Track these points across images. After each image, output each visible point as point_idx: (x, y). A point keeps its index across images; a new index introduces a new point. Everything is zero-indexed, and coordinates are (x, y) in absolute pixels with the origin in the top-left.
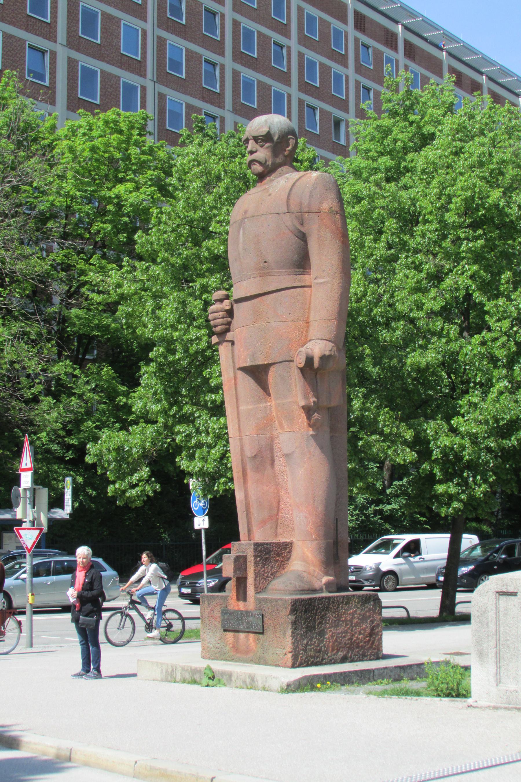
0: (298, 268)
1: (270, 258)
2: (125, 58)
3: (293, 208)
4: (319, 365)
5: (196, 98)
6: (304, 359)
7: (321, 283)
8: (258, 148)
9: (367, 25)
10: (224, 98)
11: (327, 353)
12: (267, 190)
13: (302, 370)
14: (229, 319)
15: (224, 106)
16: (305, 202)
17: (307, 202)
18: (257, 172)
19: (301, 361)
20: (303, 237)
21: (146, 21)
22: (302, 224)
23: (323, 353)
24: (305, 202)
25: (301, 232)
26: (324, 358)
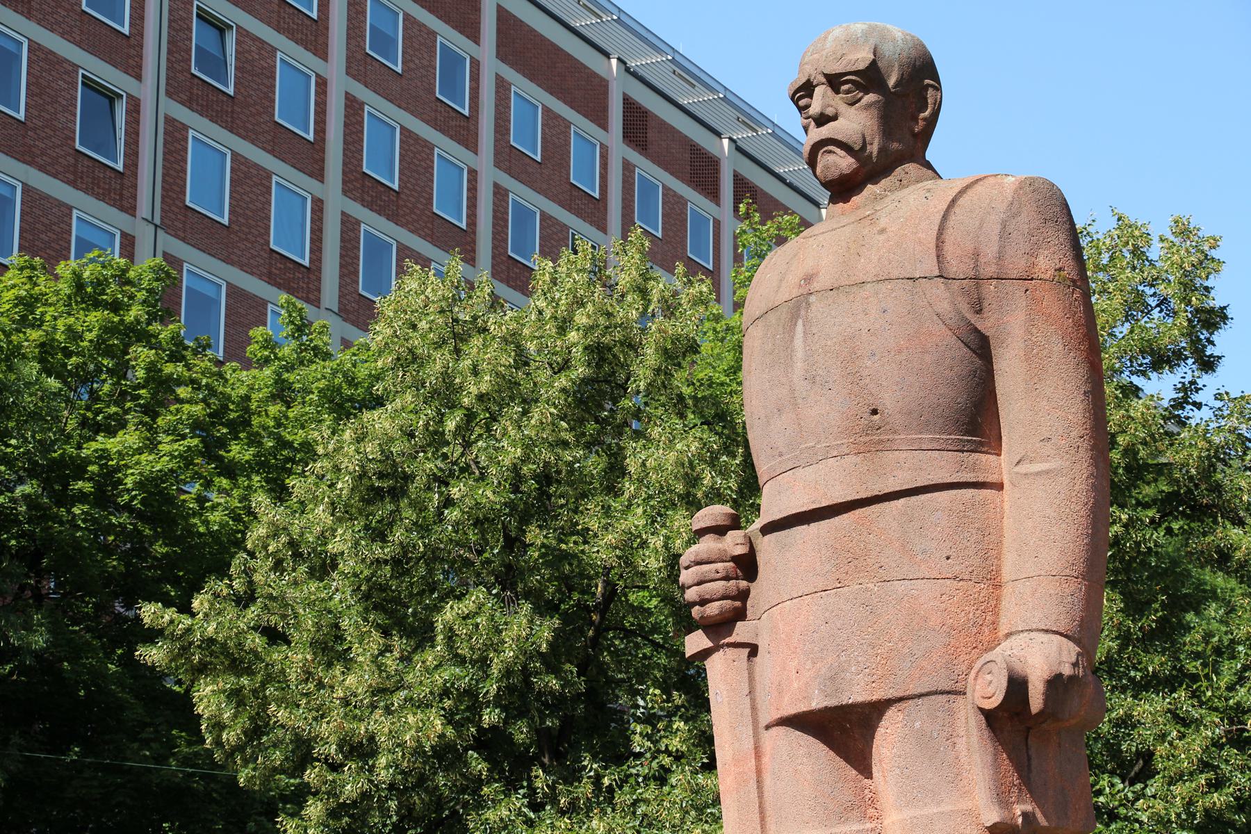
0: (967, 433)
1: (889, 401)
2: (86, 162)
3: (956, 266)
4: (1046, 701)
5: (252, 274)
6: (1004, 684)
7: (1038, 474)
8: (843, 108)
9: (651, 135)
10: (319, 279)
11: (1067, 670)
12: (872, 219)
13: (991, 717)
14: (743, 584)
15: (318, 300)
16: (990, 251)
17: (996, 248)
18: (833, 174)
19: (991, 690)
20: (981, 348)
21: (139, 77)
22: (979, 312)
23: (1056, 670)
24: (990, 251)
25: (976, 330)
26: (1055, 684)
